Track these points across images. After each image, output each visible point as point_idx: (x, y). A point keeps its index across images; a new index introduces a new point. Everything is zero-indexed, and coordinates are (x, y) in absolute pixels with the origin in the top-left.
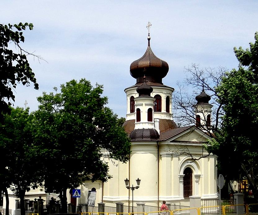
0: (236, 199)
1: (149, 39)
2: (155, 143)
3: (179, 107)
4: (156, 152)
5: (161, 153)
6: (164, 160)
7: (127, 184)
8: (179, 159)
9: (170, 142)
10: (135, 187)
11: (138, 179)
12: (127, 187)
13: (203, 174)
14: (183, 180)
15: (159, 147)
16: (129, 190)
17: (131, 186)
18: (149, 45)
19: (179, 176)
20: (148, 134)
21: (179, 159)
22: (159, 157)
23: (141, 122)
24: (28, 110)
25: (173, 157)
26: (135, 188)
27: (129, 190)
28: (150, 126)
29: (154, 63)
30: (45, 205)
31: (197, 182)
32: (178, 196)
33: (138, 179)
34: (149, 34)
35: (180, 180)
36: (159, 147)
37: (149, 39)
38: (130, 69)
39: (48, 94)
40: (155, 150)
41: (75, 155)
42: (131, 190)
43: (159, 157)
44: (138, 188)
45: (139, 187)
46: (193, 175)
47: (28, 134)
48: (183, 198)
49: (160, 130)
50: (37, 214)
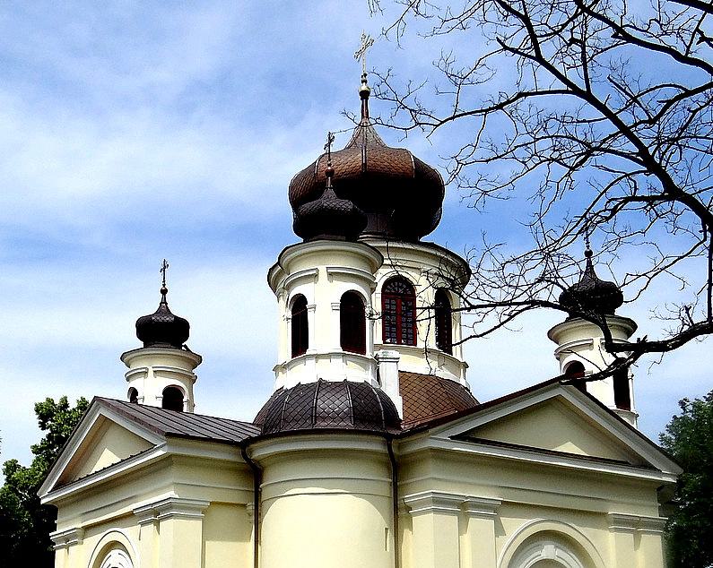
2: (375, 446)
4: (386, 490)
5: (410, 497)
6: (426, 528)
8: (499, 530)
9: (452, 438)
15: (398, 469)
20: (343, 403)
21: (499, 530)
22: (399, 515)
24: (675, 417)
25: (468, 515)
28: (355, 372)
29: (384, 162)
30: (513, 307)
34: (365, 75)
36: (398, 469)
40: (380, 480)
43: (399, 515)
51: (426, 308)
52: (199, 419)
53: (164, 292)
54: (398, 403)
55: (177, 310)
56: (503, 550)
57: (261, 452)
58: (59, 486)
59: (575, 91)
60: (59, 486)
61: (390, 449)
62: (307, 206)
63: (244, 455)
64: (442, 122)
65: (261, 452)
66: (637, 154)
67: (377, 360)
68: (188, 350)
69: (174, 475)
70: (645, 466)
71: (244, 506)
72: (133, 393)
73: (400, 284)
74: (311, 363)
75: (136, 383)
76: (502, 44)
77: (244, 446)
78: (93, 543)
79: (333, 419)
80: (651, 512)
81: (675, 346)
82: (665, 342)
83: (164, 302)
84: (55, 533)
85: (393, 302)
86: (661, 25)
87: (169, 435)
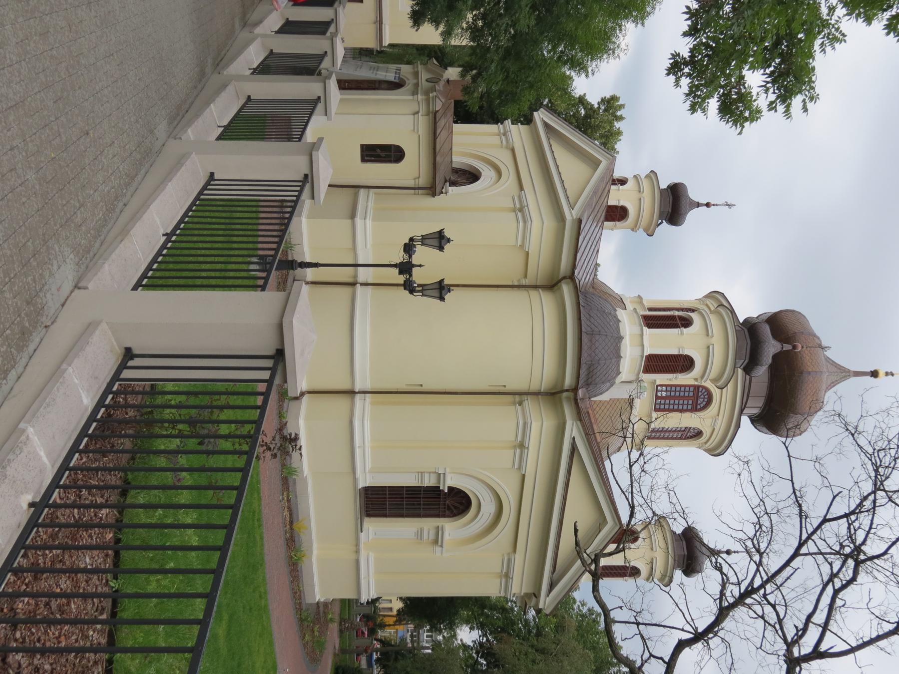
0: (219, 400)
1: (874, 374)
2: (568, 381)
4: (534, 387)
5: (530, 404)
9: (574, 438)
12: (411, 239)
18: (858, 374)
19: (441, 471)
23: (645, 328)
31: (420, 533)
32: (369, 466)
35: (427, 476)
37: (874, 374)
39: (718, 107)
46: (442, 519)
48: (361, 485)
49: (608, 402)
51: (633, 435)
52: (597, 237)
53: (708, 205)
54: (605, 397)
55: (693, 217)
56: (488, 474)
57: (566, 289)
58: (546, 125)
59: (801, 545)
60: (546, 125)
61: (567, 391)
62: (766, 330)
63: (564, 278)
64: (787, 448)
65: (566, 289)
66: (752, 587)
67: (639, 381)
68: (659, 225)
69: (550, 224)
70: (552, 586)
71: (526, 277)
72: (623, 182)
73: (706, 400)
74: (637, 330)
75: (630, 184)
76: (837, 495)
77: (571, 277)
78: (503, 158)
79: (590, 348)
80: (518, 587)
81: (595, 597)
82: (598, 591)
83: (698, 205)
84: (510, 123)
85: (691, 394)
86: (840, 607)
87: (580, 221)
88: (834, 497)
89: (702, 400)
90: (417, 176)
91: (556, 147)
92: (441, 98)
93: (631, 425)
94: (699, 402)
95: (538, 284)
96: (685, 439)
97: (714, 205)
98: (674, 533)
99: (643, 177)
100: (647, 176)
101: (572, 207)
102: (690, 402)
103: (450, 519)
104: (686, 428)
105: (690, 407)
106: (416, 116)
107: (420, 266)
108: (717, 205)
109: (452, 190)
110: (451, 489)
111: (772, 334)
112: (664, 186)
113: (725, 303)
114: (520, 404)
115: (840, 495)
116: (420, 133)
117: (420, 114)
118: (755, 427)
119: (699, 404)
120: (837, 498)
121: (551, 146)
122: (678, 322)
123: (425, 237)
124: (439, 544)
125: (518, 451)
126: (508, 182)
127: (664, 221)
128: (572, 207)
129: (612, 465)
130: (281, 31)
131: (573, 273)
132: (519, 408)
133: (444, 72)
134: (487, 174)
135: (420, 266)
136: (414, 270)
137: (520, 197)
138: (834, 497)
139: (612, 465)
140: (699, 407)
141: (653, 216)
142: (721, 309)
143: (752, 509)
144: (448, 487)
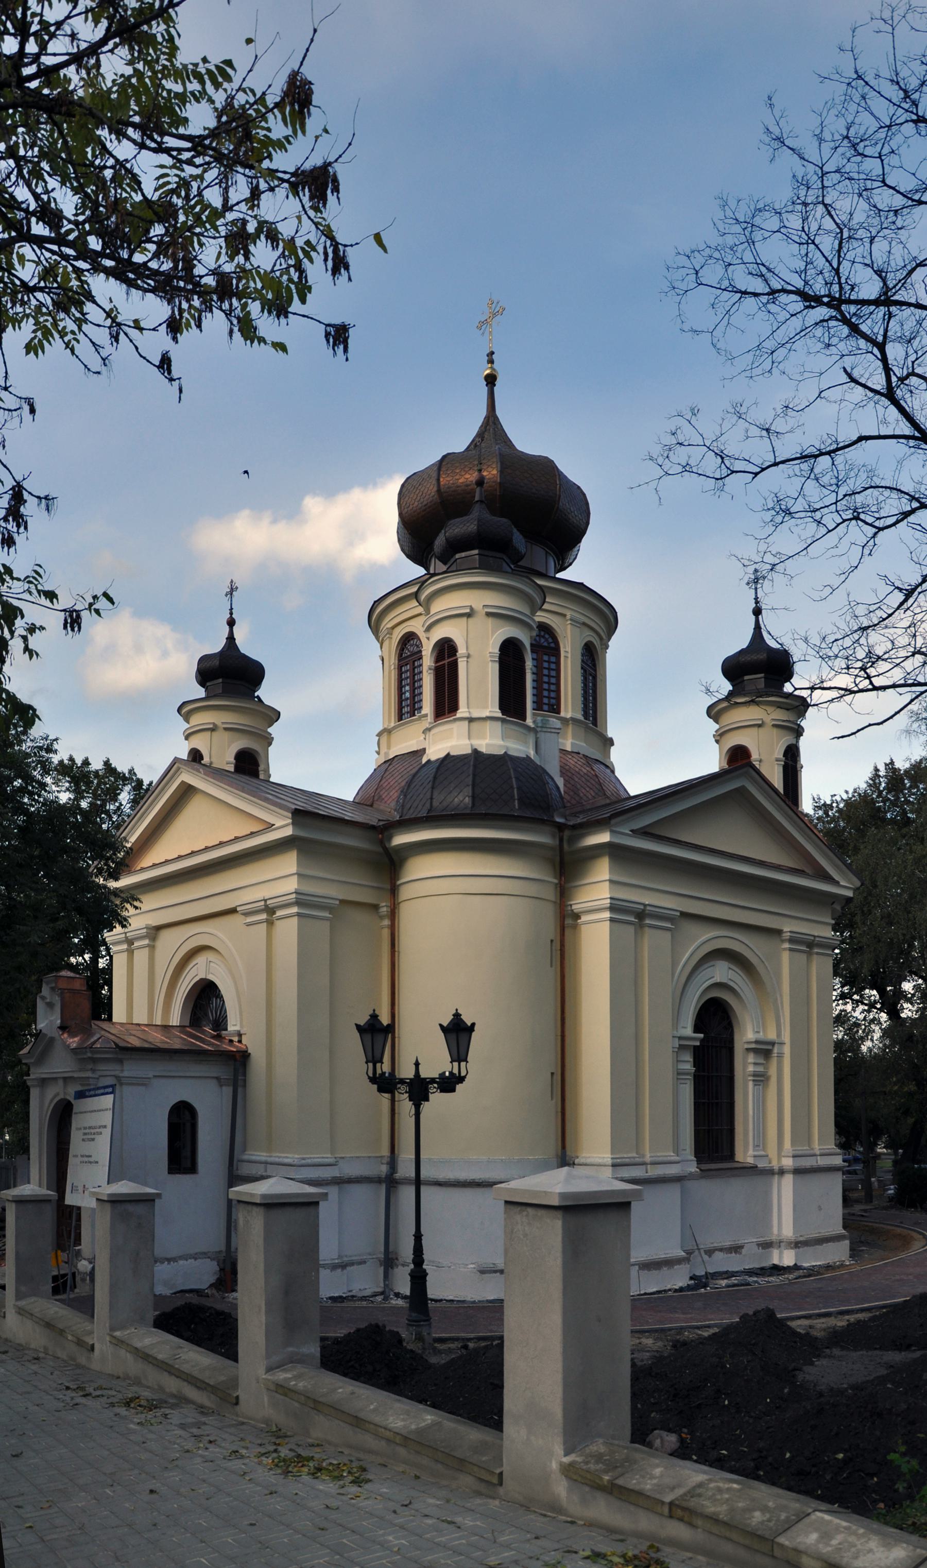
1: (491, 380)
3: (779, 519)
4: (550, 894)
7: (374, 1059)
10: (435, 1075)
11: (457, 1015)
12: (373, 1080)
13: (786, 1037)
14: (695, 1064)
16: (393, 1101)
17: (406, 1072)
26: (433, 1088)
27: (393, 1101)
33: (457, 1015)
34: (492, 353)
38: (401, 515)
41: (9, 122)
42: (406, 1106)
44: (459, 1087)
45: (461, 1079)
47: (82, 955)
50: (1, 1157)
71: (376, 907)
76: (849, 375)
88: (853, 380)
89: (543, 640)
90: (215, 1081)
91: (146, 861)
92: (92, 1040)
93: (797, 693)
94: (545, 644)
95: (388, 886)
96: (595, 671)
97: (231, 614)
98: (731, 694)
99: (187, 726)
100: (187, 718)
101: (270, 827)
102: (546, 658)
103: (736, 1030)
104: (582, 668)
105: (553, 659)
106: (124, 1081)
107: (417, 1064)
108: (231, 609)
109: (233, 1025)
110: (697, 1029)
111: (466, 515)
112: (201, 692)
113: (414, 589)
114: (577, 916)
115: (849, 370)
116: (151, 1075)
117: (121, 1075)
118: (571, 564)
119: (549, 643)
120: (855, 374)
121: (142, 869)
122: (446, 662)
123: (370, 1054)
124: (769, 1047)
125: (648, 921)
126: (220, 934)
127: (256, 694)
128: (270, 827)
129: (870, 725)
130: (742, 1247)
131: (373, 828)
132: (584, 918)
133: (45, 1035)
134: (198, 970)
135: (417, 1064)
136: (424, 1074)
137: (247, 914)
138: (853, 380)
139: (870, 725)
140: (553, 645)
141: (246, 708)
142: (423, 596)
143: (830, 531)
144: (695, 1032)
